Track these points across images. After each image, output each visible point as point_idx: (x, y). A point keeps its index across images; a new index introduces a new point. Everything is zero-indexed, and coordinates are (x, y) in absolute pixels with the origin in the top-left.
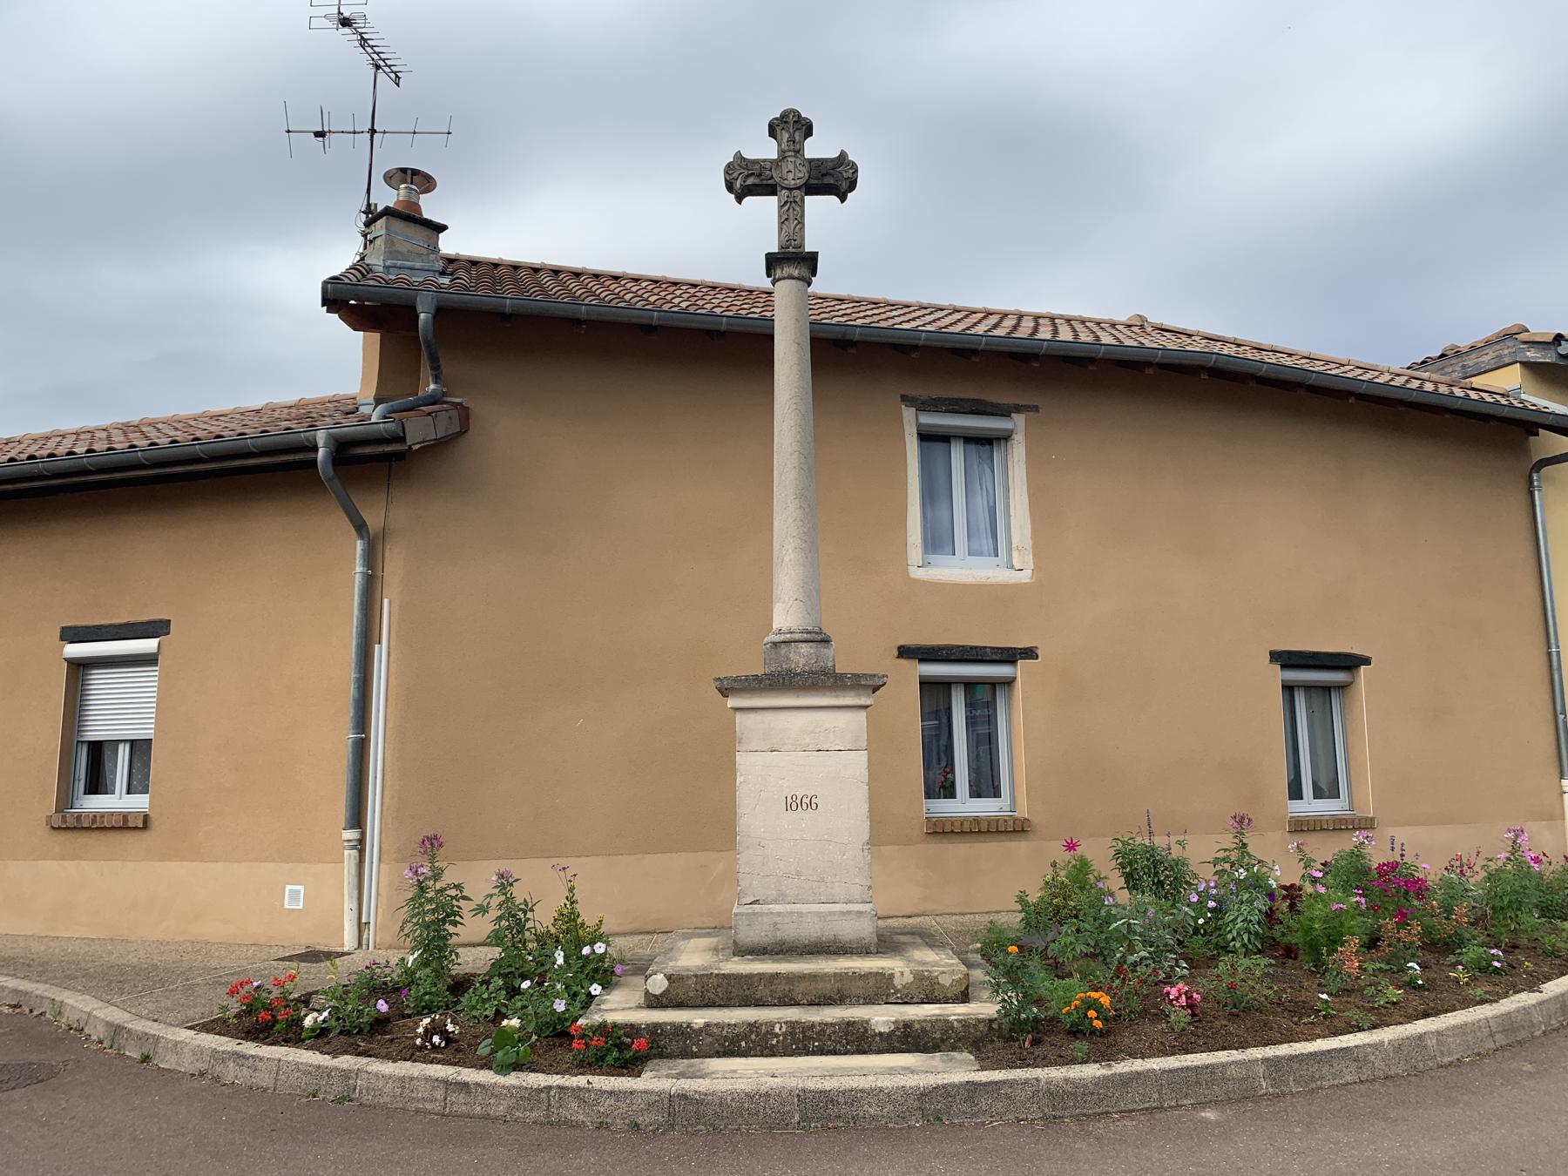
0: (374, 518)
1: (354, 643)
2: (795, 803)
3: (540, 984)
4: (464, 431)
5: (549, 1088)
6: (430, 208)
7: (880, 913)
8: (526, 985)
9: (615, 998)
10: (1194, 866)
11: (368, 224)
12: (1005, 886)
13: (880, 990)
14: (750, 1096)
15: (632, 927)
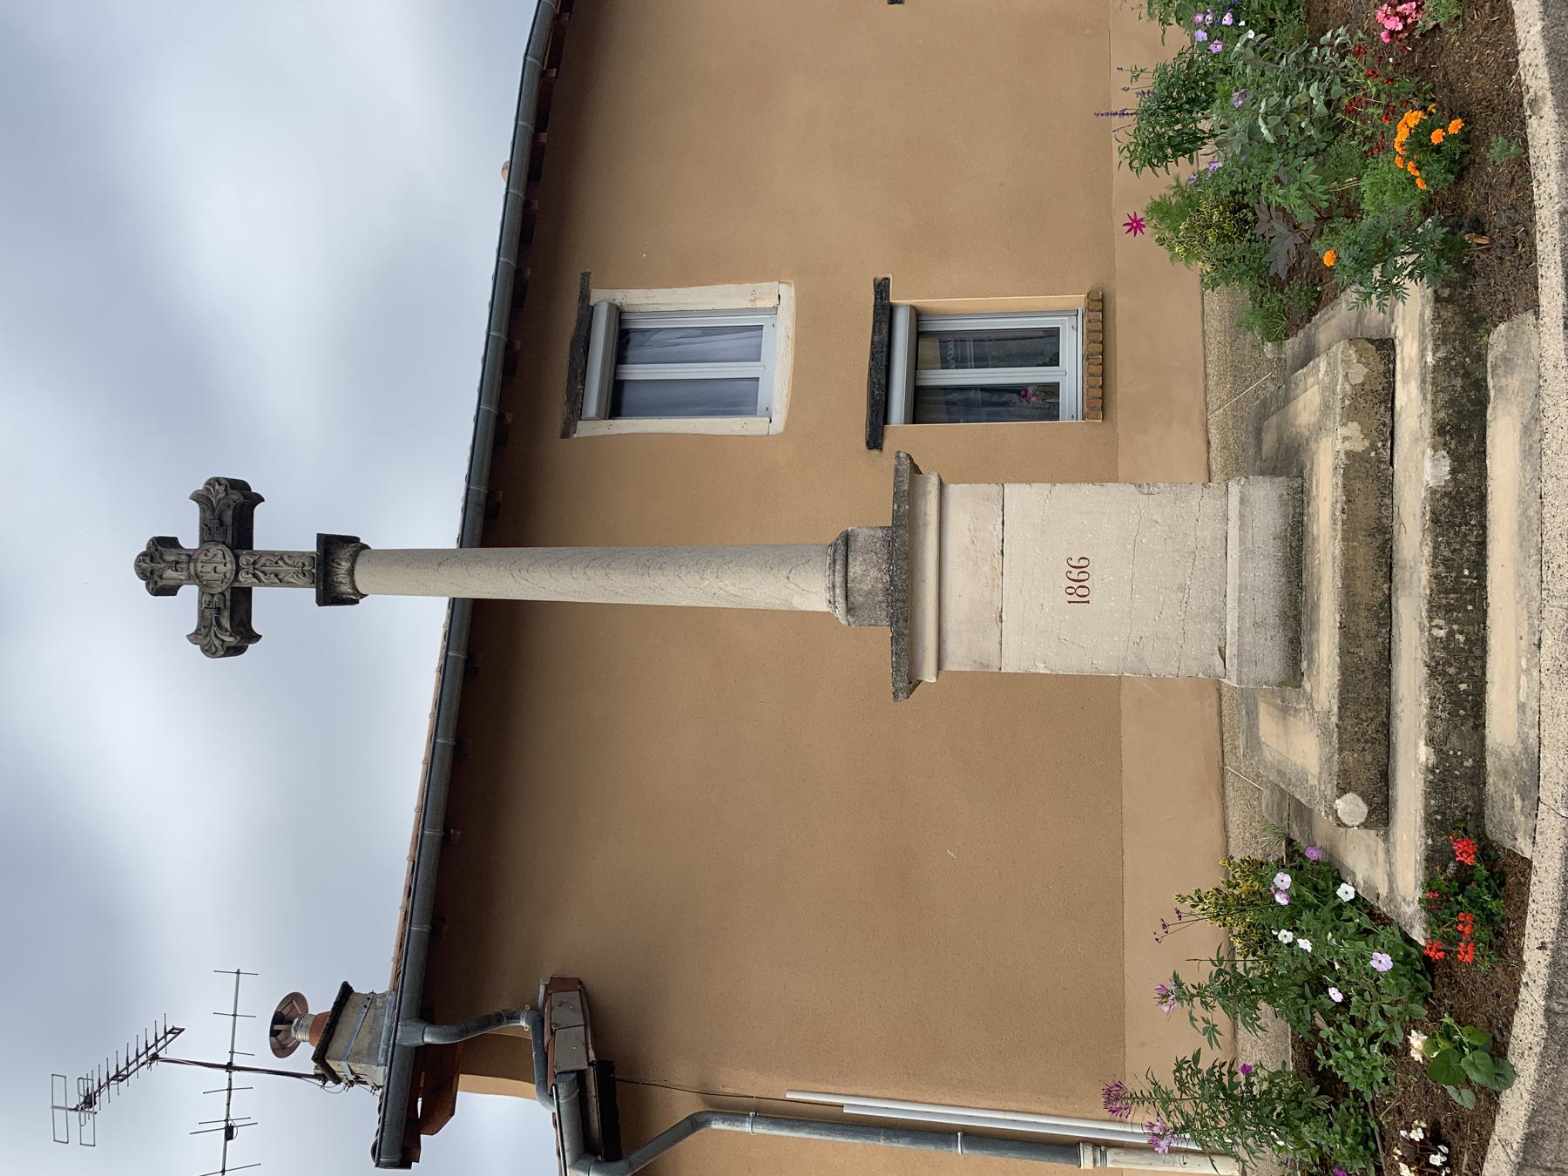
0: (684, 1105)
1: (840, 1139)
2: (1078, 585)
4: (579, 985)
6: (321, 1003)
7: (1204, 478)
10: (1169, 55)
11: (338, 1080)
12: (1181, 311)
13: (1371, 475)
15: (1214, 792)
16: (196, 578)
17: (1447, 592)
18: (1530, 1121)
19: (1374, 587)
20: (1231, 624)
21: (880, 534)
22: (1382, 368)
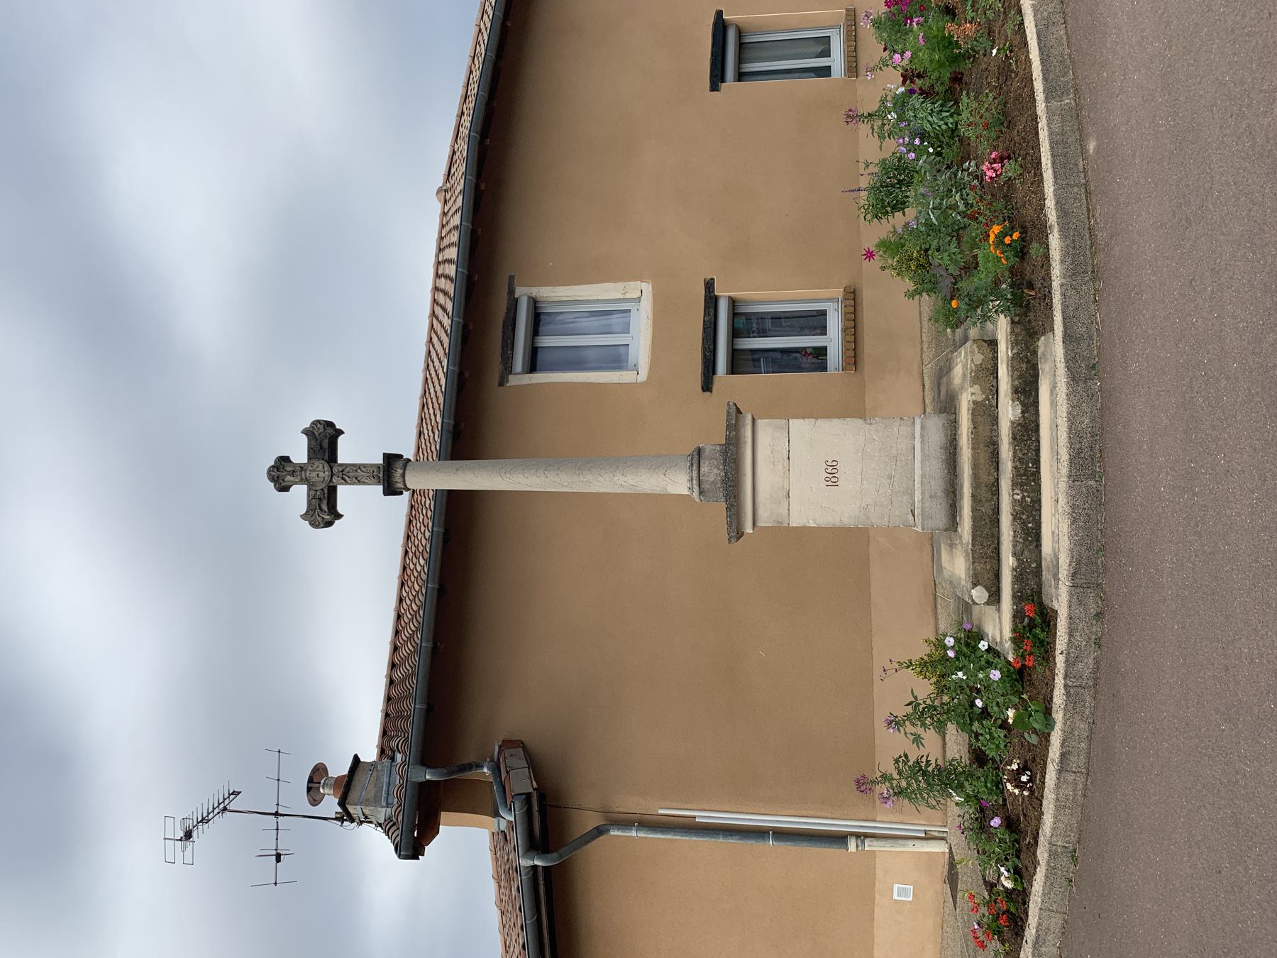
0: (591, 821)
1: (694, 839)
3: (978, 691)
4: (521, 744)
5: (1066, 686)
6: (339, 769)
8: (979, 703)
9: (991, 629)
11: (352, 820)
12: (899, 308)
13: (986, 413)
14: (1074, 521)
16: (305, 481)
18: (1062, 745)
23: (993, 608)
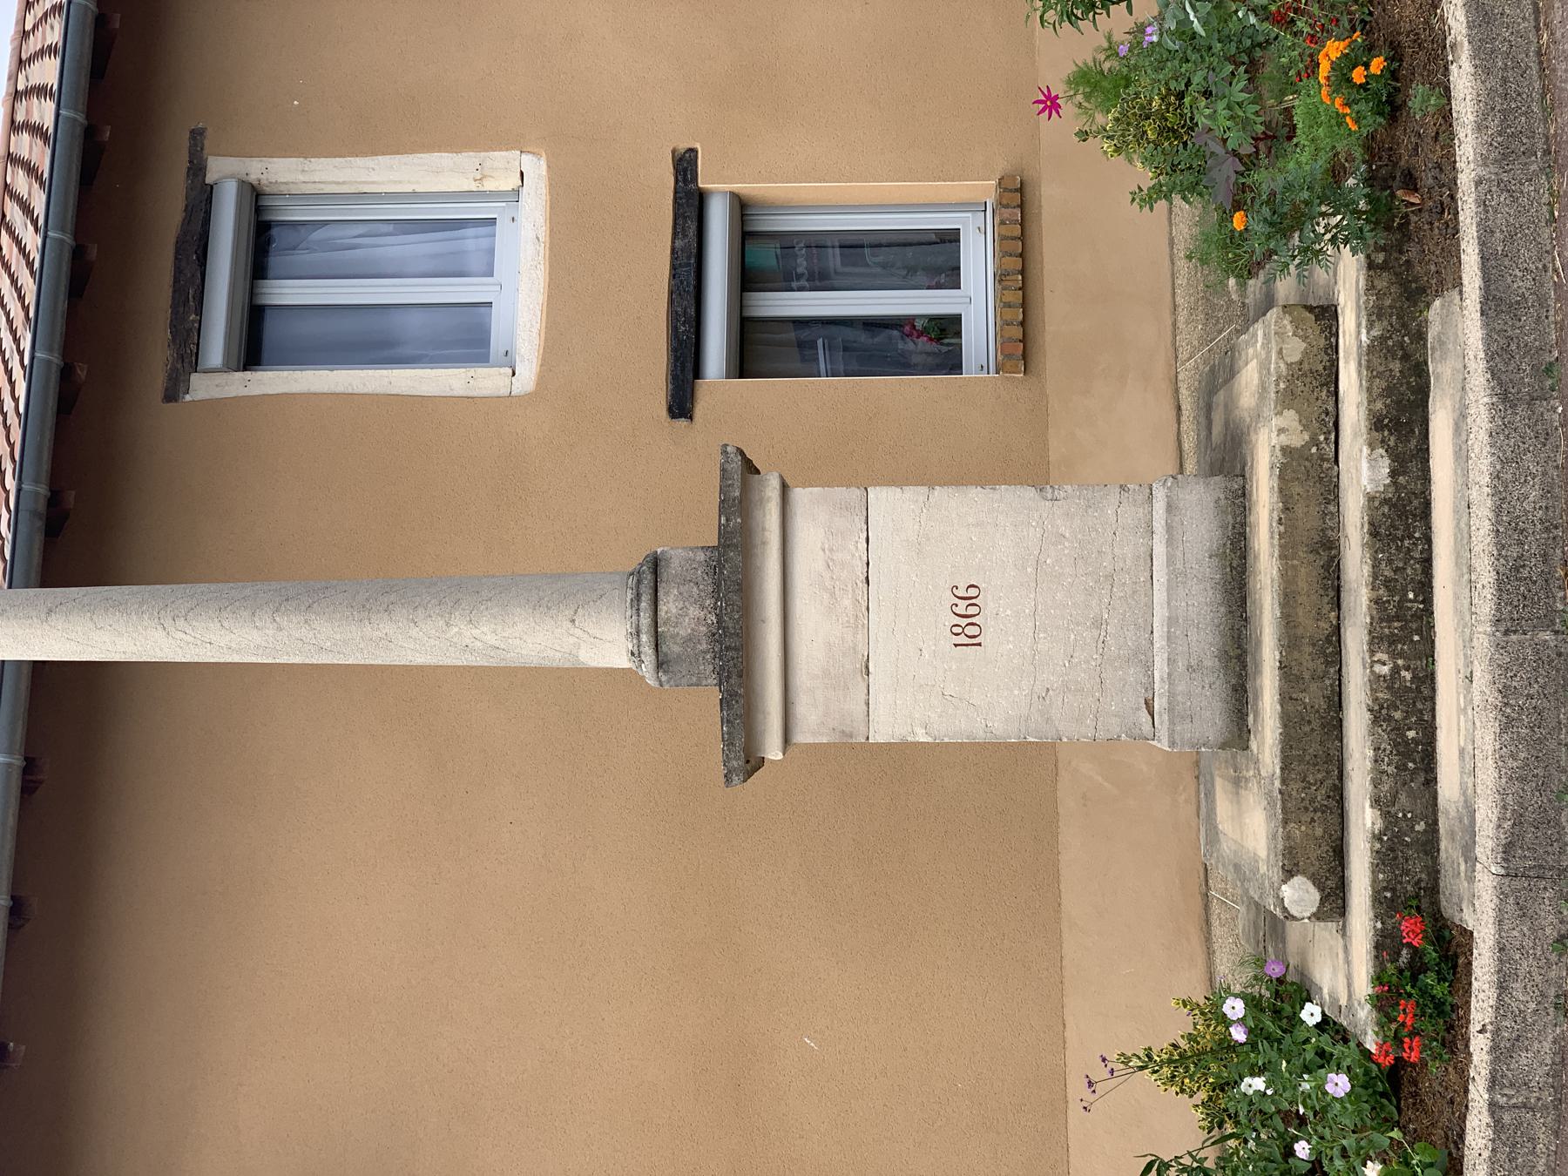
3: (1302, 1121)
5: (1493, 1107)
7: (1171, 468)
8: (1302, 1149)
9: (1326, 977)
12: (1122, 232)
13: (1313, 474)
14: (1507, 725)
17: (1390, 620)
19: (1320, 616)
20: (1160, 669)
21: (701, 556)
22: (1322, 342)
23: (1332, 926)
